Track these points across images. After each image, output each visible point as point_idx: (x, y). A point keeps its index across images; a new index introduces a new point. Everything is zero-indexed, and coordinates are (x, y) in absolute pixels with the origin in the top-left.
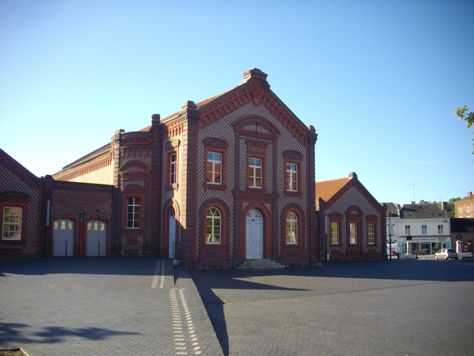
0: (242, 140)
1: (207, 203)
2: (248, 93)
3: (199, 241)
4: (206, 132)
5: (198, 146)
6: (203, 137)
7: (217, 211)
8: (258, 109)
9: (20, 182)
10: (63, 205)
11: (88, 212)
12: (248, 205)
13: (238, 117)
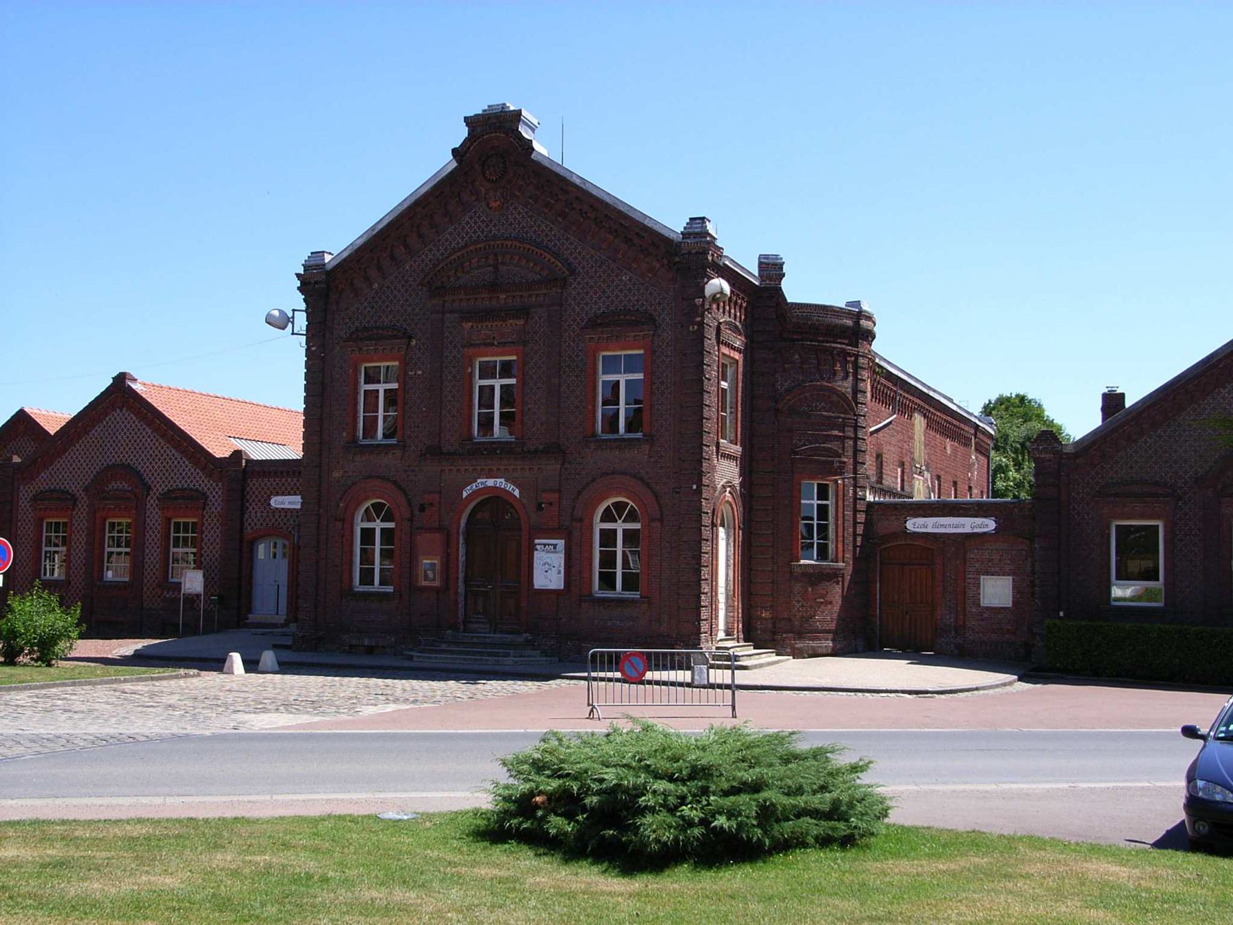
9: (192, 470)
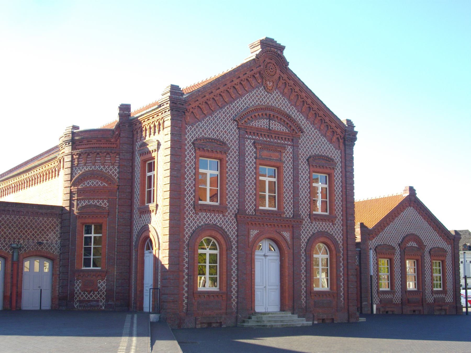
0: (249, 141)
4: (197, 130)
11: (26, 245)
12: (258, 234)
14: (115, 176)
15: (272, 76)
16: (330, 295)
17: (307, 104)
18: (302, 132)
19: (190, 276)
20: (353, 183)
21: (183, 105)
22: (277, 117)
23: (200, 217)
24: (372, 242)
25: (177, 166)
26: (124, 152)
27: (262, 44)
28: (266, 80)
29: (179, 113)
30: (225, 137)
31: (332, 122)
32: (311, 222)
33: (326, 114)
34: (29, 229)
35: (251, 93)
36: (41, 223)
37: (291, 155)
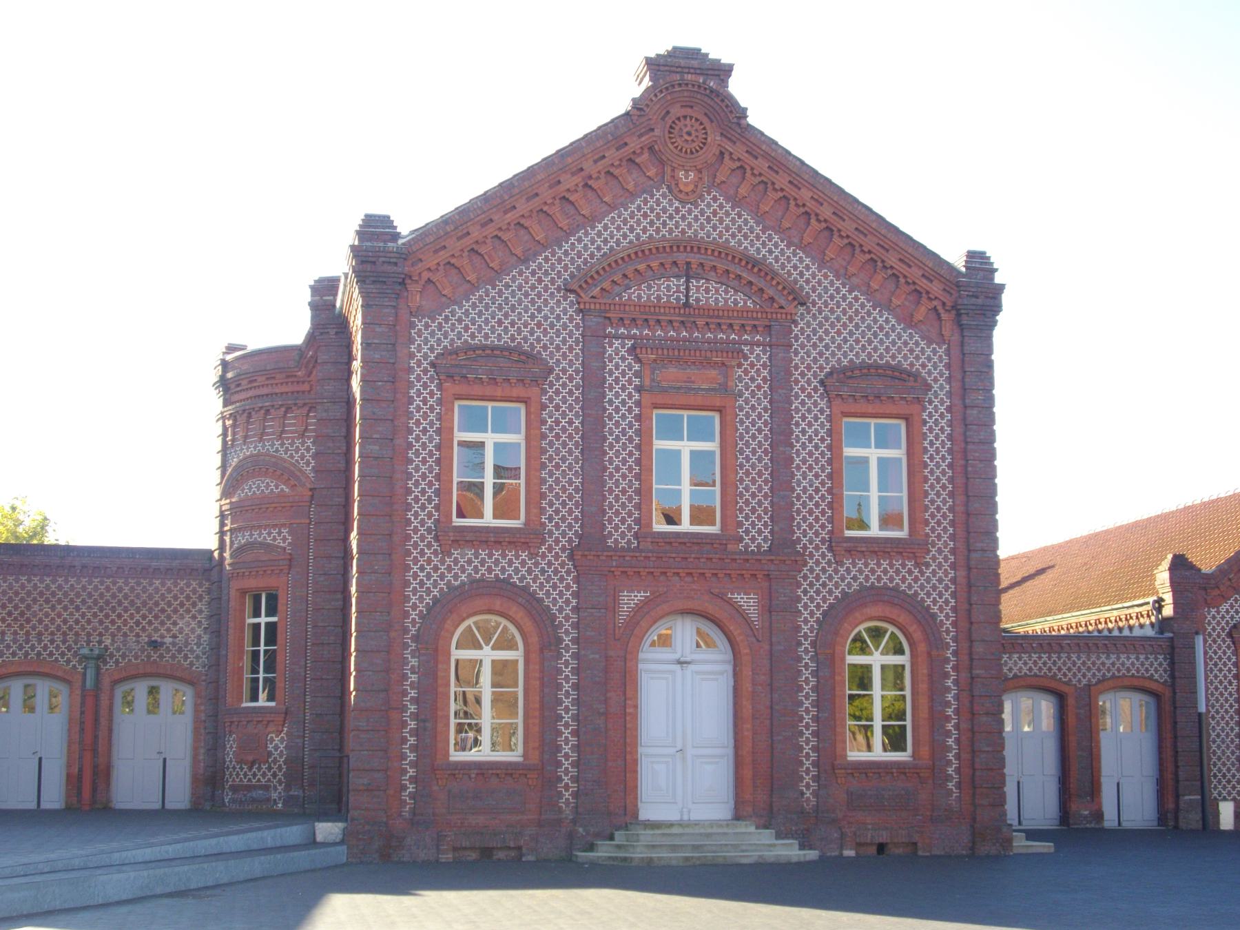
0: (617, 343)
1: (848, 605)
2: (642, 153)
3: (414, 748)
4: (447, 327)
5: (410, 385)
6: (432, 349)
7: (892, 633)
8: (696, 212)
10: (22, 628)
11: (118, 649)
12: (646, 603)
13: (598, 255)
14: (308, 466)
15: (692, 153)
16: (905, 773)
17: (819, 221)
18: (802, 304)
19: (424, 721)
20: (993, 441)
21: (396, 264)
22: (714, 268)
23: (456, 562)
24: (1218, 612)
25: (381, 429)
26: (325, 401)
27: (653, 67)
28: (671, 166)
29: (385, 287)
30: (539, 340)
31: (911, 263)
32: (836, 562)
33: (887, 241)
34: (126, 610)
35: (626, 210)
36: (157, 593)
37: (765, 373)
